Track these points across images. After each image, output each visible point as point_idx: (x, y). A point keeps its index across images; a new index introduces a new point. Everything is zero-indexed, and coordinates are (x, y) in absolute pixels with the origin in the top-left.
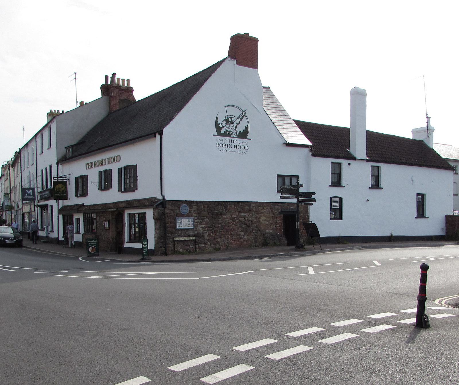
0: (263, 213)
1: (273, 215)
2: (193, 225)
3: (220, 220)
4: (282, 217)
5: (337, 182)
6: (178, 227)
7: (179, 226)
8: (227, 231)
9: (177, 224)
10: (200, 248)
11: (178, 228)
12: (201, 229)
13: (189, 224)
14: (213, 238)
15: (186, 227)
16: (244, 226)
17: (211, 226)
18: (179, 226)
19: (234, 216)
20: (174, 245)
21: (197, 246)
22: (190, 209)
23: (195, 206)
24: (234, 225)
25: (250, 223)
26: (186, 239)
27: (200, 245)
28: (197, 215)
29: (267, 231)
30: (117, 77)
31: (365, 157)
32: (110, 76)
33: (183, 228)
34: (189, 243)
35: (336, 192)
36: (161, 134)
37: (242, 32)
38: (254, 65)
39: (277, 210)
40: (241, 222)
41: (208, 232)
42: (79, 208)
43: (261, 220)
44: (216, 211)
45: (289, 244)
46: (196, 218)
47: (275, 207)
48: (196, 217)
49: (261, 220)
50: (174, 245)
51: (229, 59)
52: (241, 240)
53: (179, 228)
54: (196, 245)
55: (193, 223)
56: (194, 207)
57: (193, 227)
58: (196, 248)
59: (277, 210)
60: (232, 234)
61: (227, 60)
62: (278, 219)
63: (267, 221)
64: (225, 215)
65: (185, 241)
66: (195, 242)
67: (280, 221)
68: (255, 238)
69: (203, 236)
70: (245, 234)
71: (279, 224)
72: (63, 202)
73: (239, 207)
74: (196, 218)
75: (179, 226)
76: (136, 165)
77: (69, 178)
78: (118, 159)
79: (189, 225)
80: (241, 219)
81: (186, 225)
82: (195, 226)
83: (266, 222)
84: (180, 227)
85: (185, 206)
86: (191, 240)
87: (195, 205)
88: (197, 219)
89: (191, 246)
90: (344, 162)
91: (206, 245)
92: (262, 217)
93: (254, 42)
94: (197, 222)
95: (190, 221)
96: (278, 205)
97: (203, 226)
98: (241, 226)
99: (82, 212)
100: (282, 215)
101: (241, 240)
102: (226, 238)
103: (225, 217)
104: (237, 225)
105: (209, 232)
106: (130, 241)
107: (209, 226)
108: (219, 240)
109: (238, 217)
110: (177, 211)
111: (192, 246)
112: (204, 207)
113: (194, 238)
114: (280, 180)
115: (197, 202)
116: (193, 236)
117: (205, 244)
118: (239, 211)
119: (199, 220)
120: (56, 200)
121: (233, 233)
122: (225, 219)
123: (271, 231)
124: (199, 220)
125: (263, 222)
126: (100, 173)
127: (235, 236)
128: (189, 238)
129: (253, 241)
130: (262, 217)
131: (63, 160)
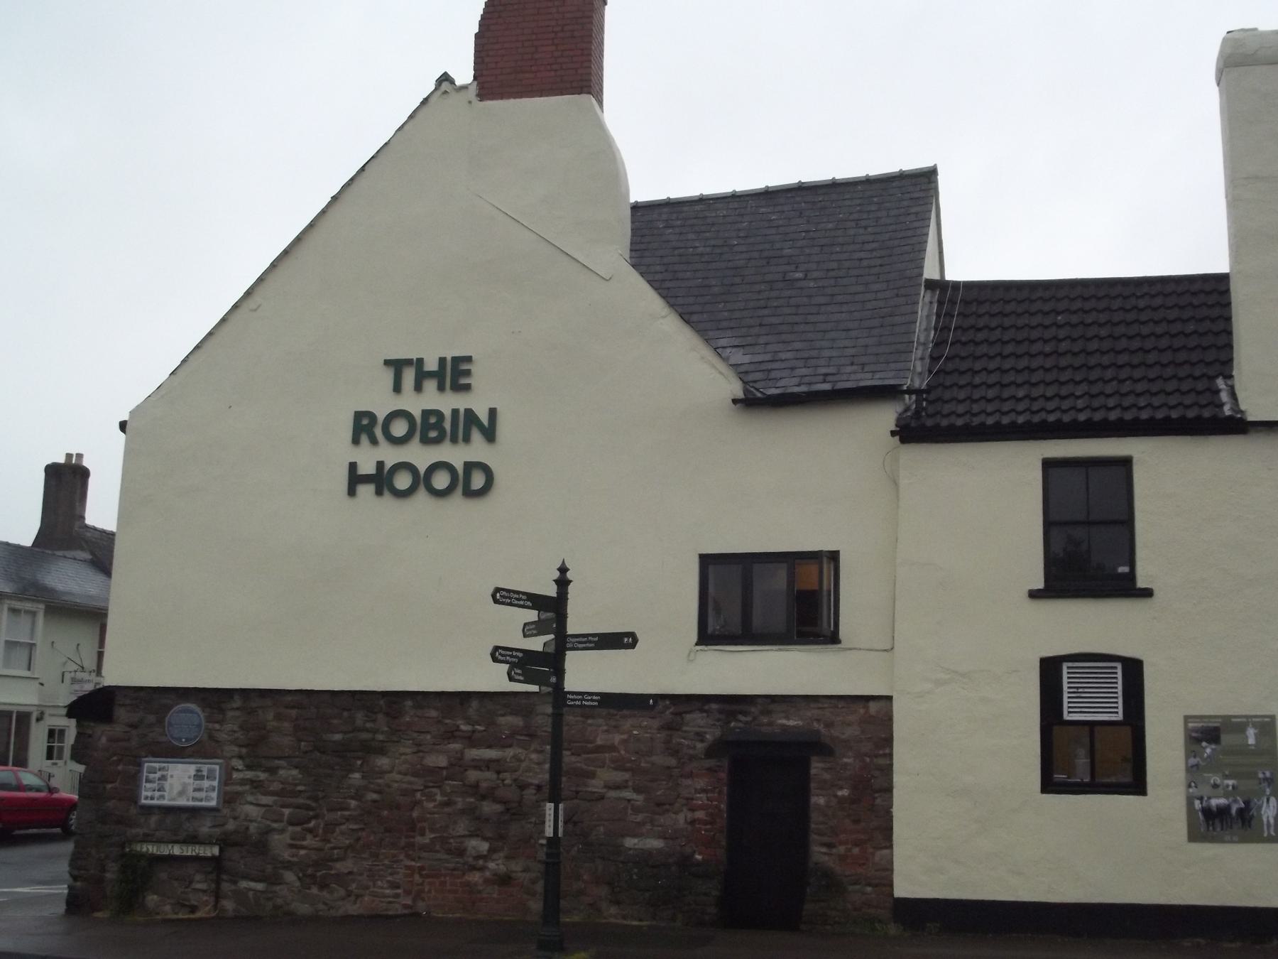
0: (612, 748)
2: (214, 795)
3: (357, 775)
6: (146, 798)
7: (148, 795)
8: (388, 830)
9: (144, 784)
11: (143, 801)
13: (195, 790)
15: (182, 802)
16: (488, 808)
17: (309, 802)
18: (149, 794)
19: (438, 760)
21: (226, 887)
22: (210, 725)
23: (237, 713)
24: (431, 805)
27: (244, 884)
28: (244, 750)
33: (165, 802)
38: (597, 93)
39: (700, 736)
41: (290, 828)
43: (595, 785)
44: (338, 737)
46: (241, 762)
47: (688, 717)
48: (240, 757)
53: (149, 802)
54: (218, 882)
55: (215, 783)
56: (230, 714)
57: (213, 803)
61: (433, 100)
62: (701, 783)
63: (637, 790)
64: (382, 751)
71: (701, 808)
73: (468, 720)
74: (238, 764)
75: (148, 795)
76: (839, 551)
77: (503, 596)
79: (198, 795)
80: (473, 775)
81: (182, 793)
82: (229, 799)
83: (628, 794)
84: (152, 798)
85: (192, 712)
87: (237, 709)
88: (240, 767)
89: (199, 886)
91: (277, 888)
92: (599, 772)
94: (243, 782)
95: (205, 773)
96: (702, 711)
98: (470, 812)
102: (386, 862)
103: (383, 762)
104: (448, 803)
105: (298, 829)
107: (301, 801)
109: (458, 766)
112: (279, 717)
115: (245, 693)
118: (470, 738)
119: (249, 775)
120: (567, 652)
122: (382, 773)
123: (655, 844)
124: (249, 775)
125: (613, 794)
127: (439, 856)
128: (189, 851)
130: (599, 772)
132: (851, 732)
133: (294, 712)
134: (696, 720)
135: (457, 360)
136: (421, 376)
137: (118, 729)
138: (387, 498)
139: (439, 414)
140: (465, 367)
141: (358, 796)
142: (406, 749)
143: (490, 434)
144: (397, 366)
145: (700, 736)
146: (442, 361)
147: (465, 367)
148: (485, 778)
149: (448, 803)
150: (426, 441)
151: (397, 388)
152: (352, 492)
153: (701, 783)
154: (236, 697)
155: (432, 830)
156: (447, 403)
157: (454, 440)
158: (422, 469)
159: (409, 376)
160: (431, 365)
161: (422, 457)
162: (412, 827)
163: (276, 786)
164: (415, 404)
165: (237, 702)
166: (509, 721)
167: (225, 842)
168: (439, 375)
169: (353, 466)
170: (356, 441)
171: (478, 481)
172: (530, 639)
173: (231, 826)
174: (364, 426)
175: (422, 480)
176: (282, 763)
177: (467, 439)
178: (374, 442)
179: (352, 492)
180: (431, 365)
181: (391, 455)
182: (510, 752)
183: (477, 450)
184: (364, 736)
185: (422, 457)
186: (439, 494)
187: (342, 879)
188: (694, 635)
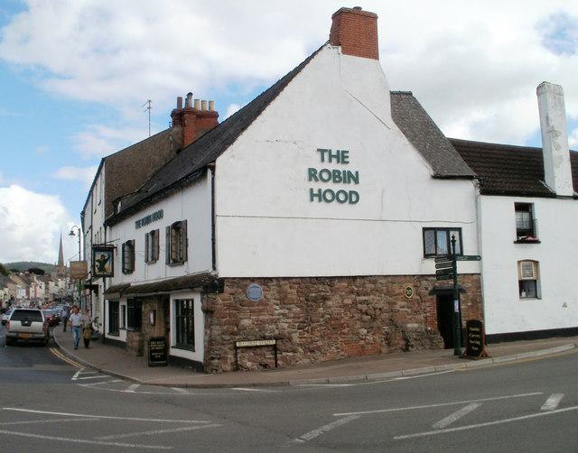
1: (418, 297)
4: (435, 300)
5: (527, 234)
10: (284, 359)
12: (286, 326)
14: (309, 340)
16: (366, 318)
19: (348, 301)
20: (236, 355)
25: (378, 312)
26: (258, 343)
27: (284, 354)
29: (409, 325)
30: (194, 97)
31: (570, 191)
32: (184, 97)
34: (264, 350)
35: (529, 252)
36: (213, 169)
37: (351, 6)
40: (361, 311)
42: (124, 289)
43: (397, 307)
44: (314, 295)
45: (448, 346)
49: (397, 307)
50: (236, 355)
51: (333, 53)
52: (362, 342)
54: (276, 354)
58: (276, 360)
59: (427, 289)
60: (344, 334)
61: (325, 48)
65: (257, 347)
66: (275, 348)
67: (430, 308)
68: (386, 339)
69: (290, 339)
70: (368, 332)
72: (110, 281)
78: (159, 215)
80: (359, 306)
83: (406, 309)
86: (267, 346)
90: (539, 204)
93: (371, 19)
97: (290, 321)
98: (361, 320)
99: (198, 292)
100: (435, 296)
101: (362, 342)
103: (329, 303)
104: (353, 317)
108: (320, 343)
109: (355, 303)
110: (242, 297)
111: (269, 355)
113: (273, 342)
114: (430, 234)
116: (270, 338)
117: (294, 351)
119: (282, 311)
121: (345, 331)
123: (416, 325)
125: (401, 310)
129: (384, 343)
131: (112, 221)
132: (470, 285)
133: (296, 286)
134: (424, 283)
135: (344, 152)
136: (331, 157)
137: (226, 295)
138: (323, 202)
139: (339, 172)
140: (345, 155)
141: (323, 317)
142: (337, 297)
143: (357, 181)
144: (322, 151)
145: (427, 289)
146: (338, 151)
147: (345, 155)
148: (364, 307)
149: (353, 317)
150: (335, 181)
151: (323, 160)
152: (312, 200)
153: (428, 304)
154: (274, 280)
155: (348, 327)
156: (341, 168)
157: (345, 182)
158: (335, 192)
159: (326, 156)
160: (334, 153)
161: (336, 188)
162: (342, 326)
163: (292, 315)
164: (327, 165)
165: (275, 282)
166: (369, 286)
167: (276, 338)
168: (337, 157)
169: (312, 190)
170: (310, 180)
171: (354, 199)
172: (23, 349)
173: (277, 332)
174: (313, 174)
175: (335, 197)
176: (293, 306)
177: (349, 182)
178: (316, 180)
179: (312, 200)
180: (334, 153)
181: (324, 187)
182: (371, 297)
183: (317, 186)
184: (323, 294)
185: (336, 188)
186: (329, 201)
187: (319, 348)
188: (421, 254)
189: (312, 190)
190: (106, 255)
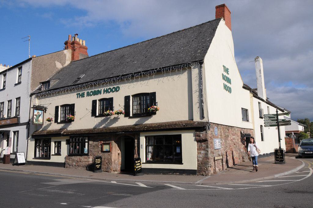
76: (113, 98)
106: (148, 162)
126: (94, 102)
151: (78, 97)
189: (104, 89)
190: (40, 112)
